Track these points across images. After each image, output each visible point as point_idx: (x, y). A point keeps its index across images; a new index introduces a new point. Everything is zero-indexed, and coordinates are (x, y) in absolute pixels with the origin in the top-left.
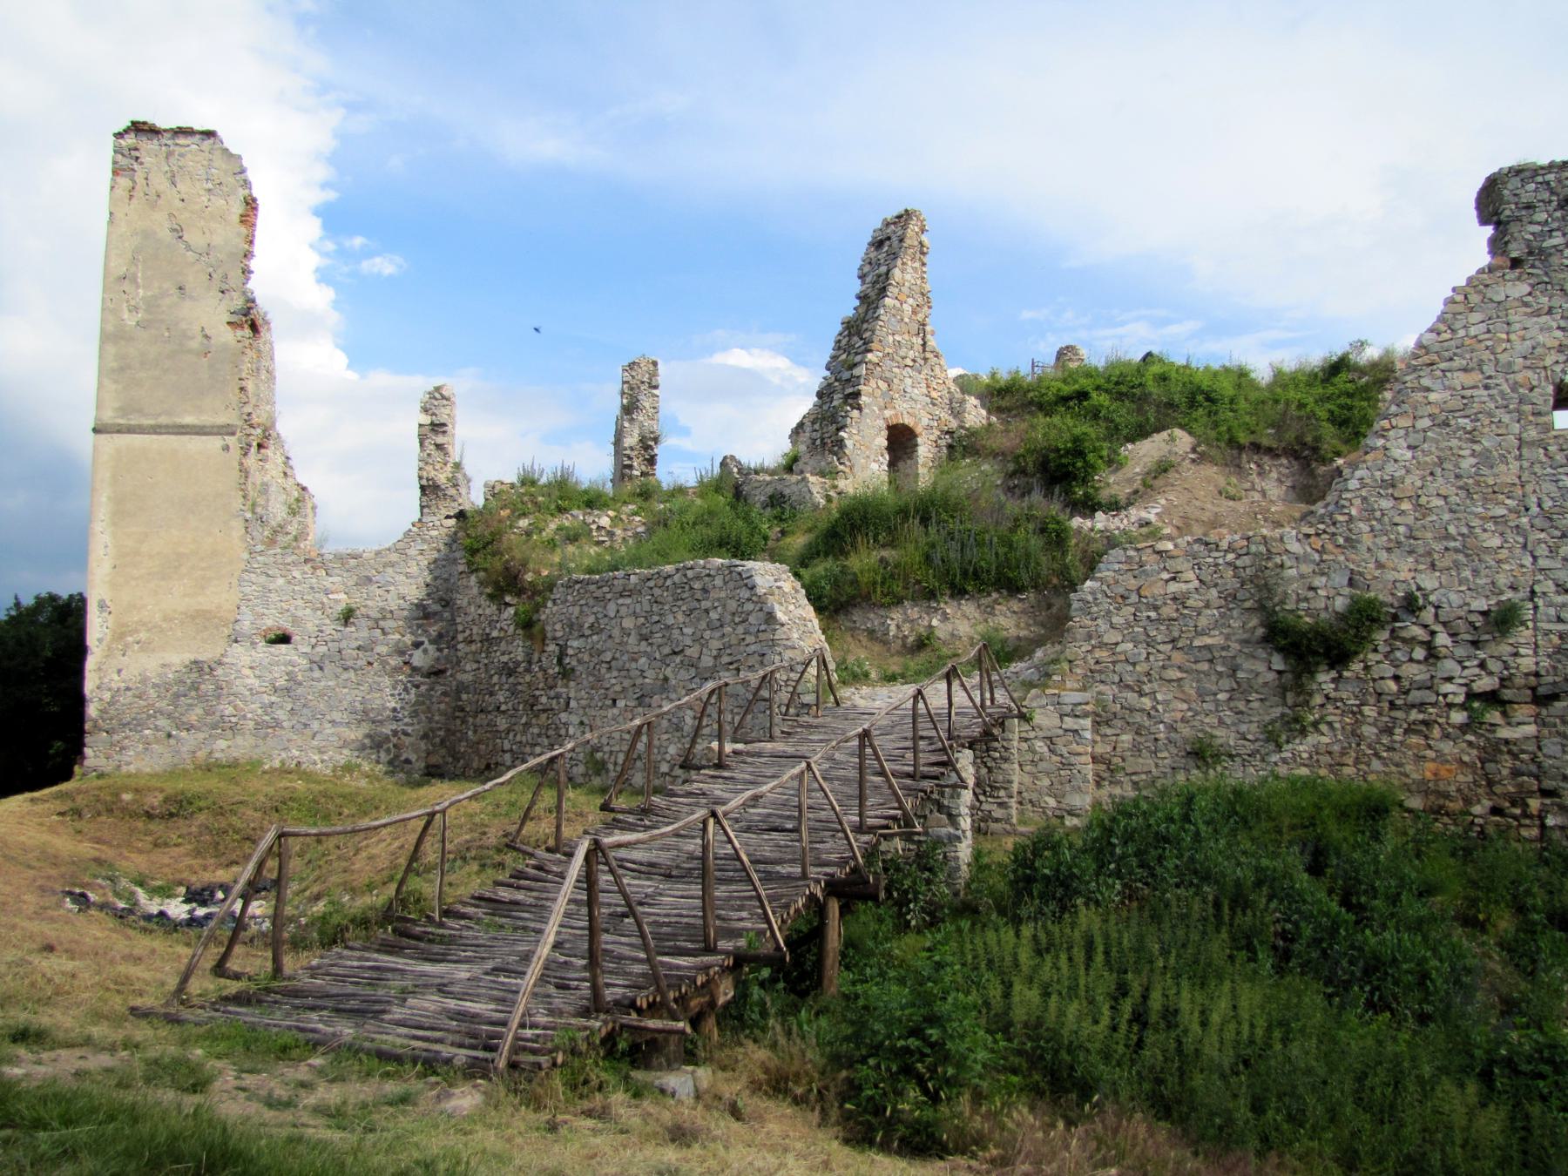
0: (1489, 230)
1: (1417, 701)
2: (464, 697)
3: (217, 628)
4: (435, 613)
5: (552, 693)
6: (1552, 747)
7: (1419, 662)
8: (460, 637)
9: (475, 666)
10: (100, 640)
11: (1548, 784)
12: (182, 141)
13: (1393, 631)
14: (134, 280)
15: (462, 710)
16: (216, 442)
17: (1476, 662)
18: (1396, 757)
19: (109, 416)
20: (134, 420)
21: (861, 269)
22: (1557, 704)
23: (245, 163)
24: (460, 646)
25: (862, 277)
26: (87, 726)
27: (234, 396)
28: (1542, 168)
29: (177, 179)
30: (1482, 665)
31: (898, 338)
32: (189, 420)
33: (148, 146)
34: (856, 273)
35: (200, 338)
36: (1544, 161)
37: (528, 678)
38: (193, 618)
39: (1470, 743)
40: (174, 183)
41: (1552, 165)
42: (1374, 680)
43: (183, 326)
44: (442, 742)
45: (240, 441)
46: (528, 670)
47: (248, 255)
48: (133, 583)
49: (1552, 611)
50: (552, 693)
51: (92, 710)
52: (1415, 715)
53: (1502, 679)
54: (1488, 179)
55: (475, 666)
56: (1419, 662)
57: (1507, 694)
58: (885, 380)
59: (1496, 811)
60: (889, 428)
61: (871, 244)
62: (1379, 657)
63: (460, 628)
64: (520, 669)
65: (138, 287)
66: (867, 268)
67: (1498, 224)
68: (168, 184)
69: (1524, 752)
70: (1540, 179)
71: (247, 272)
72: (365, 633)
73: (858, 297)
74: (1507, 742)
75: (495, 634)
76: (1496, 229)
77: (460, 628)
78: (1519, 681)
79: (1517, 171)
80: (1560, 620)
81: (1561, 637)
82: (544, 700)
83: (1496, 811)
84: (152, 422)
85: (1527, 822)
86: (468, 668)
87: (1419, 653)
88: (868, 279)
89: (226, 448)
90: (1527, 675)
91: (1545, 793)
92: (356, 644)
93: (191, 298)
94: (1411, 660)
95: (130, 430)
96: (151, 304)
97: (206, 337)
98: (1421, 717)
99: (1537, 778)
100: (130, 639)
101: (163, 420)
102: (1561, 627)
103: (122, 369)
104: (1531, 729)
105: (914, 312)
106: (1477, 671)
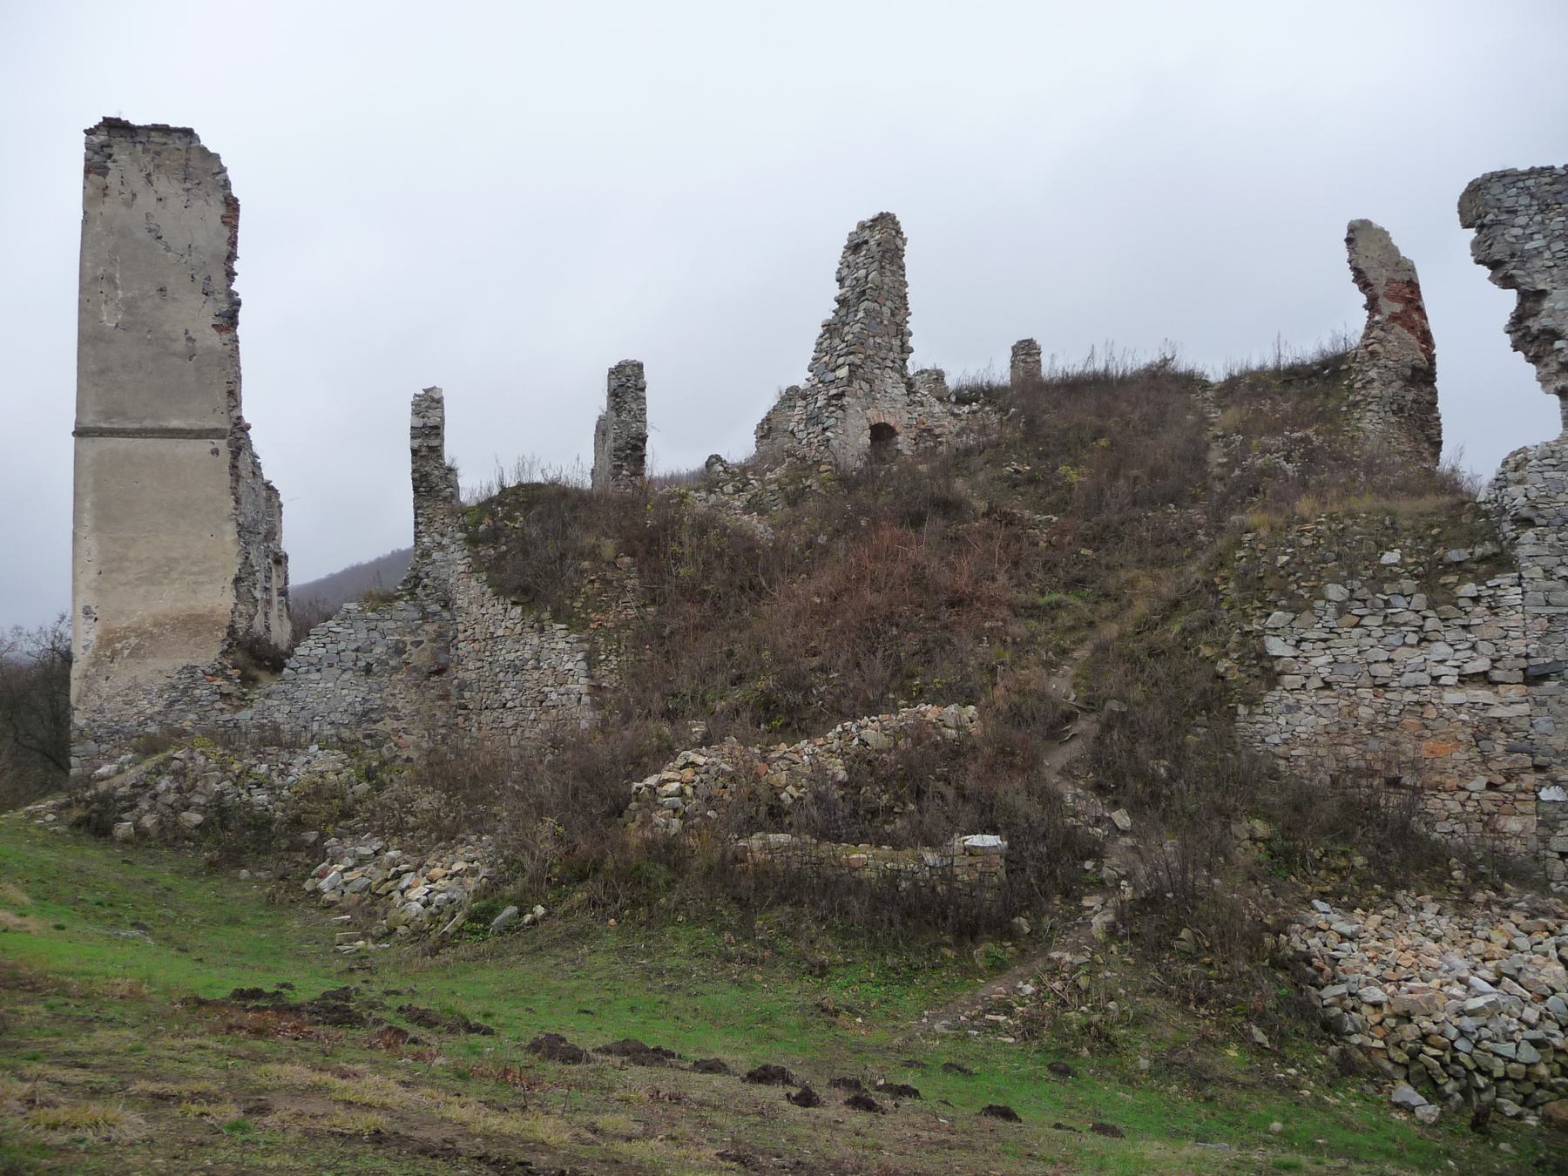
0: (1472, 233)
1: (1412, 684)
2: (467, 694)
3: (211, 632)
4: (435, 614)
5: (562, 690)
6: (1543, 724)
7: (1412, 646)
8: (461, 637)
9: (479, 664)
10: (85, 648)
11: (1540, 760)
12: (1371, 276)
13: (1386, 617)
14: (111, 280)
15: (466, 708)
16: (205, 446)
17: (1468, 645)
18: (1393, 736)
19: (89, 421)
20: (117, 424)
21: (839, 272)
22: (1547, 684)
23: (224, 162)
24: (461, 645)
25: (840, 280)
26: (74, 735)
27: (222, 400)
28: (1523, 174)
29: (153, 178)
30: (1473, 648)
31: (878, 340)
32: (175, 423)
33: (122, 152)
34: (834, 276)
35: (183, 340)
36: (1523, 166)
37: (536, 675)
38: (185, 623)
39: (1464, 722)
40: (150, 182)
41: (1532, 171)
42: (1369, 664)
43: (167, 327)
44: (444, 738)
45: (230, 445)
46: (537, 668)
47: (232, 257)
48: (121, 589)
49: (1540, 596)
50: (562, 690)
51: (79, 719)
52: (1409, 696)
53: (1493, 661)
54: (1471, 184)
55: (479, 664)
56: (1412, 646)
57: (1497, 675)
58: (867, 381)
59: (1491, 786)
60: (872, 428)
61: (847, 248)
62: (1371, 641)
63: (461, 627)
64: (529, 667)
65: (116, 288)
66: (845, 272)
67: (1481, 228)
68: (143, 182)
69: (1517, 730)
70: (1521, 184)
71: (231, 275)
72: (363, 635)
73: (838, 301)
74: (1500, 720)
75: (500, 632)
76: (1479, 232)
77: (461, 627)
78: (1509, 662)
79: (1503, 175)
80: (1548, 603)
81: (1550, 621)
82: (554, 696)
83: (1491, 786)
84: (137, 426)
85: (1522, 796)
86: (471, 666)
87: (1412, 639)
88: (847, 283)
89: (215, 452)
90: (1517, 656)
91: (1539, 768)
92: (354, 646)
93: (175, 300)
94: (1404, 644)
95: (101, 433)
96: (130, 306)
97: (190, 339)
98: (1415, 698)
99: (1531, 754)
100: (118, 646)
101: (148, 424)
102: (1551, 610)
103: (102, 372)
104: (1524, 709)
105: (893, 315)
106: (1469, 653)
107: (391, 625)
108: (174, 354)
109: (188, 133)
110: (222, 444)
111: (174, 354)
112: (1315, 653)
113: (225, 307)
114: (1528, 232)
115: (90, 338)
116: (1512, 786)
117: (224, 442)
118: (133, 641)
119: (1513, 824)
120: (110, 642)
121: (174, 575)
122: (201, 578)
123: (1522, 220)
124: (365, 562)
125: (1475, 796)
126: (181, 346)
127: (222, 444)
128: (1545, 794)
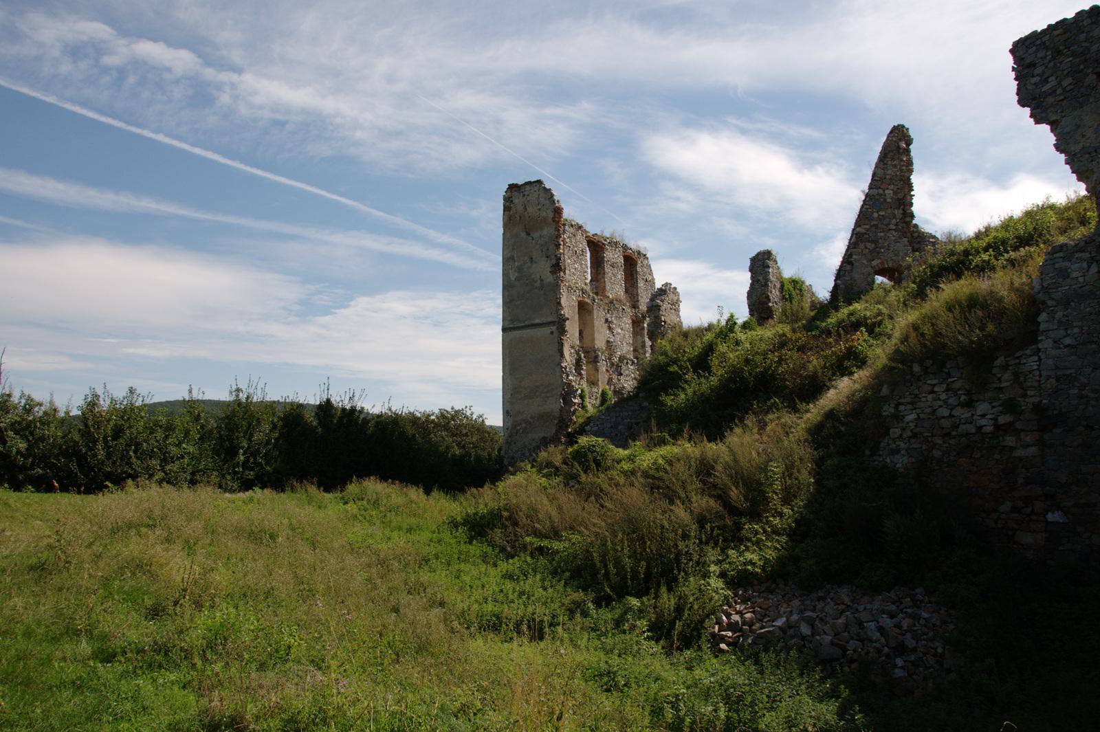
16: (547, 330)
32: (537, 321)
62: (940, 403)
81: (1058, 380)
84: (523, 325)
89: (552, 333)
93: (536, 262)
107: (626, 414)
108: (536, 288)
109: (539, 182)
110: (554, 328)
111: (536, 288)
112: (906, 413)
113: (554, 262)
114: (1043, 77)
115: (861, 211)
116: (1028, 510)
117: (555, 327)
118: (524, 425)
119: (1027, 539)
120: (516, 426)
121: (538, 394)
122: (548, 395)
123: (1039, 70)
124: (373, 405)
125: (1004, 516)
126: (538, 284)
127: (554, 328)
128: (1051, 517)
